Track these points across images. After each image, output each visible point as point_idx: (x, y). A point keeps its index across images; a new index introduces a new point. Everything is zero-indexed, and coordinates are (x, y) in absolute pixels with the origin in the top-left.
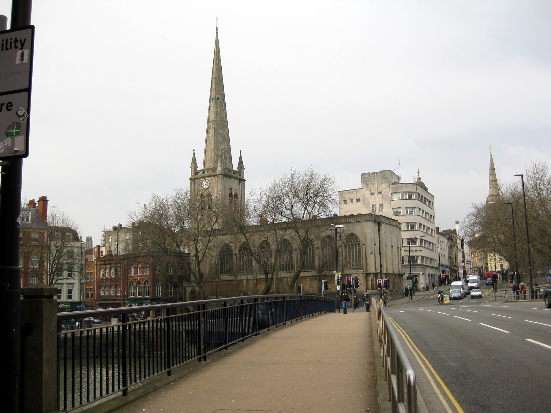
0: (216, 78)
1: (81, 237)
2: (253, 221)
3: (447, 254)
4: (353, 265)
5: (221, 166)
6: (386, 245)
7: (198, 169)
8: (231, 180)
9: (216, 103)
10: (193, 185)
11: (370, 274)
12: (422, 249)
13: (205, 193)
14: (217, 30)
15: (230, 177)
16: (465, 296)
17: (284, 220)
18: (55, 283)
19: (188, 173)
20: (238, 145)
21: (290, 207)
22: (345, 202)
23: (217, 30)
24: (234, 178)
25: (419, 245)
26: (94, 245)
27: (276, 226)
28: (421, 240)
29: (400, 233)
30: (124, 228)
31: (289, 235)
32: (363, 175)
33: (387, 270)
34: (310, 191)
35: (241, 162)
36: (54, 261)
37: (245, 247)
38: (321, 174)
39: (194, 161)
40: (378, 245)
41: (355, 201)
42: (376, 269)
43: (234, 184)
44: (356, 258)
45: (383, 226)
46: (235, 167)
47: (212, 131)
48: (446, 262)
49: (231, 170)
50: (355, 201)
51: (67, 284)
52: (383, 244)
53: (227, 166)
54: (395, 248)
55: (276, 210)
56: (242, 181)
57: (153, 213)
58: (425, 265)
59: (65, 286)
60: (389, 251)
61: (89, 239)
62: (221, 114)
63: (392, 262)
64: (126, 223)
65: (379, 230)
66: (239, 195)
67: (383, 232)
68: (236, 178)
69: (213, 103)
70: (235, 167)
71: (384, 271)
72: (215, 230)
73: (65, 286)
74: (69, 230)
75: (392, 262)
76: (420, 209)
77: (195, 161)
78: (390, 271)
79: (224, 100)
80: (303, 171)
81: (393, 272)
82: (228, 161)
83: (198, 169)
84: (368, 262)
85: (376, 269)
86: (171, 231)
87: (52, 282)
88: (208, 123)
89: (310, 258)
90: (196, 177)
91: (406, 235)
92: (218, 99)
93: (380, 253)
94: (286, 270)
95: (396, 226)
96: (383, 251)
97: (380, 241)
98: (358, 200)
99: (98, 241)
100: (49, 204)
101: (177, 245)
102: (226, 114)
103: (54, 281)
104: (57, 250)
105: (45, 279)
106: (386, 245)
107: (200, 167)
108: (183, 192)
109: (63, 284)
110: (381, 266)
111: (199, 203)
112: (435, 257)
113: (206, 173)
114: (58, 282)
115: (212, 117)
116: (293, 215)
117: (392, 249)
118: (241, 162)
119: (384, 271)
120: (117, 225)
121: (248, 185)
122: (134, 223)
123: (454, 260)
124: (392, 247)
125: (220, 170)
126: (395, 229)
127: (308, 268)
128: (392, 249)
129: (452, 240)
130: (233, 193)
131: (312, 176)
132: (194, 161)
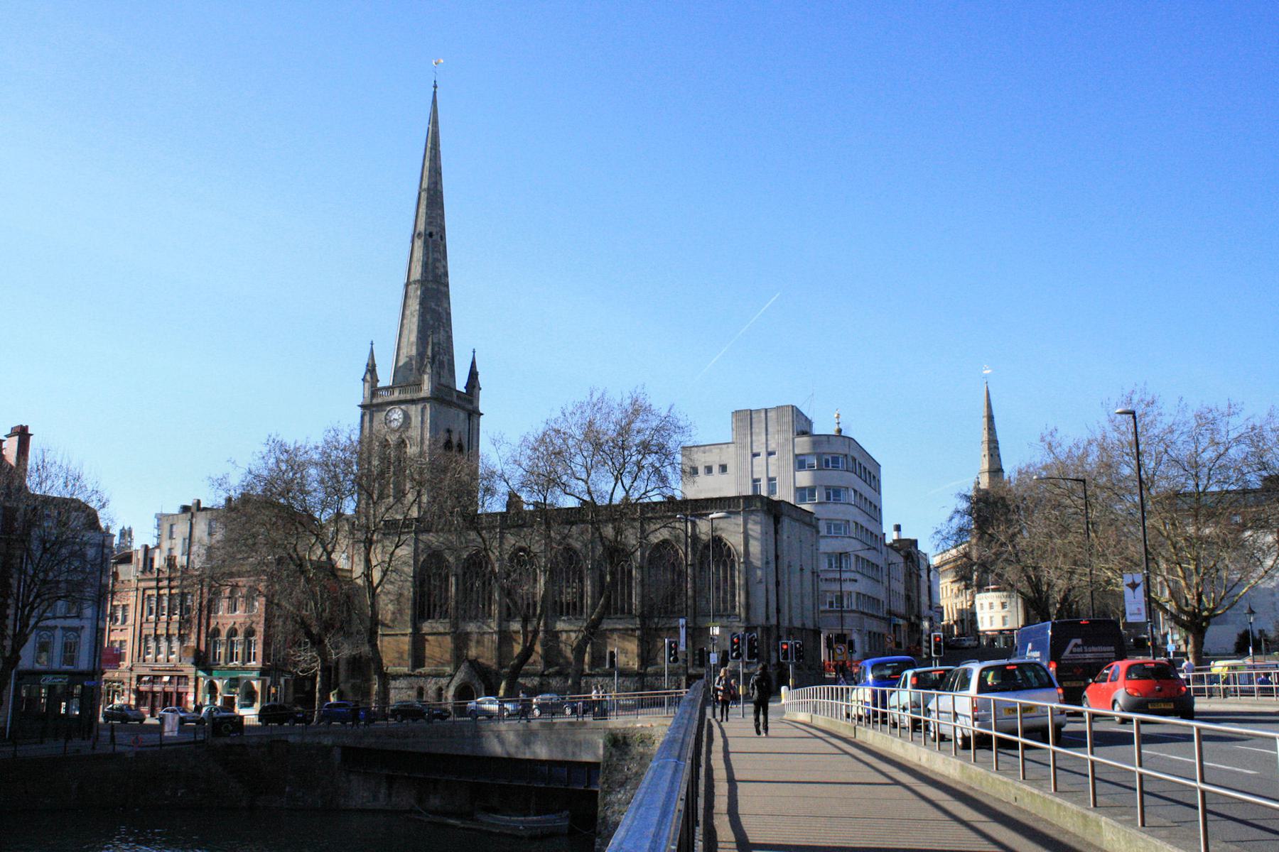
0: (428, 189)
1: (108, 528)
2: (496, 505)
3: (902, 592)
4: (725, 609)
5: (434, 382)
6: (789, 566)
7: (379, 385)
8: (453, 411)
9: (425, 242)
10: (367, 418)
11: (756, 628)
12: (858, 576)
13: (392, 439)
14: (435, 87)
15: (450, 404)
16: (250, 642)
17: (571, 503)
18: (35, 626)
19: (358, 393)
20: (468, 339)
21: (584, 476)
22: (695, 471)
23: (435, 87)
24: (458, 406)
25: (853, 568)
26: (137, 545)
27: (546, 515)
28: (857, 557)
29: (817, 541)
30: (205, 509)
31: (578, 537)
32: (737, 413)
33: (790, 620)
34: (632, 439)
35: (473, 375)
36: (35, 574)
37: (476, 564)
38: (659, 404)
39: (371, 369)
40: (773, 566)
41: (716, 469)
42: (767, 618)
43: (458, 420)
44: (725, 593)
45: (786, 523)
46: (461, 384)
47: (414, 305)
48: (900, 607)
49: (451, 388)
50: (716, 469)
51: (63, 628)
52: (785, 561)
53: (443, 381)
54: (807, 573)
55: (551, 481)
56: (474, 414)
57: (270, 483)
58: (862, 613)
59: (58, 634)
60: (796, 579)
61: (126, 533)
62: (435, 268)
63: (802, 602)
64: (213, 498)
65: (776, 532)
66: (466, 447)
67: (785, 537)
68: (464, 409)
69: (419, 243)
70: (461, 384)
71: (785, 623)
72: (411, 519)
73: (58, 634)
74: (83, 508)
75: (802, 602)
76: (855, 491)
77: (374, 366)
78: (797, 624)
79: (443, 238)
80: (618, 395)
81: (803, 625)
82: (446, 370)
83: (379, 385)
84: (751, 601)
85: (767, 618)
86: (311, 517)
87: (27, 625)
88: (407, 285)
89: (623, 588)
90: (375, 401)
91: (828, 545)
92: (431, 235)
93: (778, 584)
94: (568, 614)
95: (810, 525)
96: (784, 578)
97: (777, 557)
98: (724, 468)
99: (144, 536)
100: (33, 442)
101: (325, 550)
102: (445, 267)
103: (32, 622)
104: (45, 550)
105: (11, 617)
106: (789, 566)
107: (385, 378)
108: (343, 439)
109: (56, 627)
110: (778, 611)
111: (374, 467)
112: (882, 596)
113: (396, 394)
114: (40, 624)
115: (417, 273)
116: (589, 493)
117: (802, 575)
118: (473, 375)
119: (785, 623)
120: (189, 504)
121: (487, 427)
122: (229, 500)
123: (916, 605)
124: (802, 570)
125: (426, 388)
126: (807, 532)
127: (623, 612)
128: (802, 575)
129: (913, 561)
130: (455, 440)
131: (638, 410)
132: (371, 369)
